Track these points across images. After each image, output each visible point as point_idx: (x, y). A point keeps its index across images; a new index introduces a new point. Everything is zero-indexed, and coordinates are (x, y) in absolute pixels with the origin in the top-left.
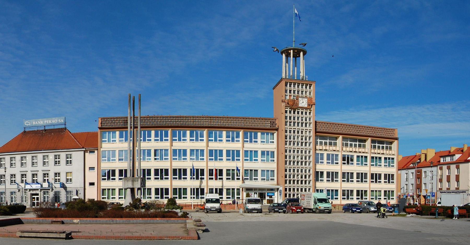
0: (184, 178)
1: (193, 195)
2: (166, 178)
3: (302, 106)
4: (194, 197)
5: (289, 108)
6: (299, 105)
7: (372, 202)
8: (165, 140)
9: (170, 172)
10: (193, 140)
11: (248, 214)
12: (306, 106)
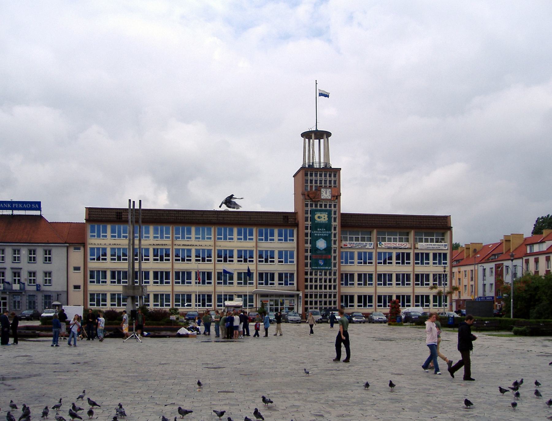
0: (271, 284)
1: (198, 302)
2: (167, 283)
3: (325, 198)
4: (200, 305)
5: (328, 201)
6: (321, 197)
7: (177, 309)
8: (250, 239)
9: (374, 277)
10: (115, 236)
11: (360, 324)
12: (330, 198)
